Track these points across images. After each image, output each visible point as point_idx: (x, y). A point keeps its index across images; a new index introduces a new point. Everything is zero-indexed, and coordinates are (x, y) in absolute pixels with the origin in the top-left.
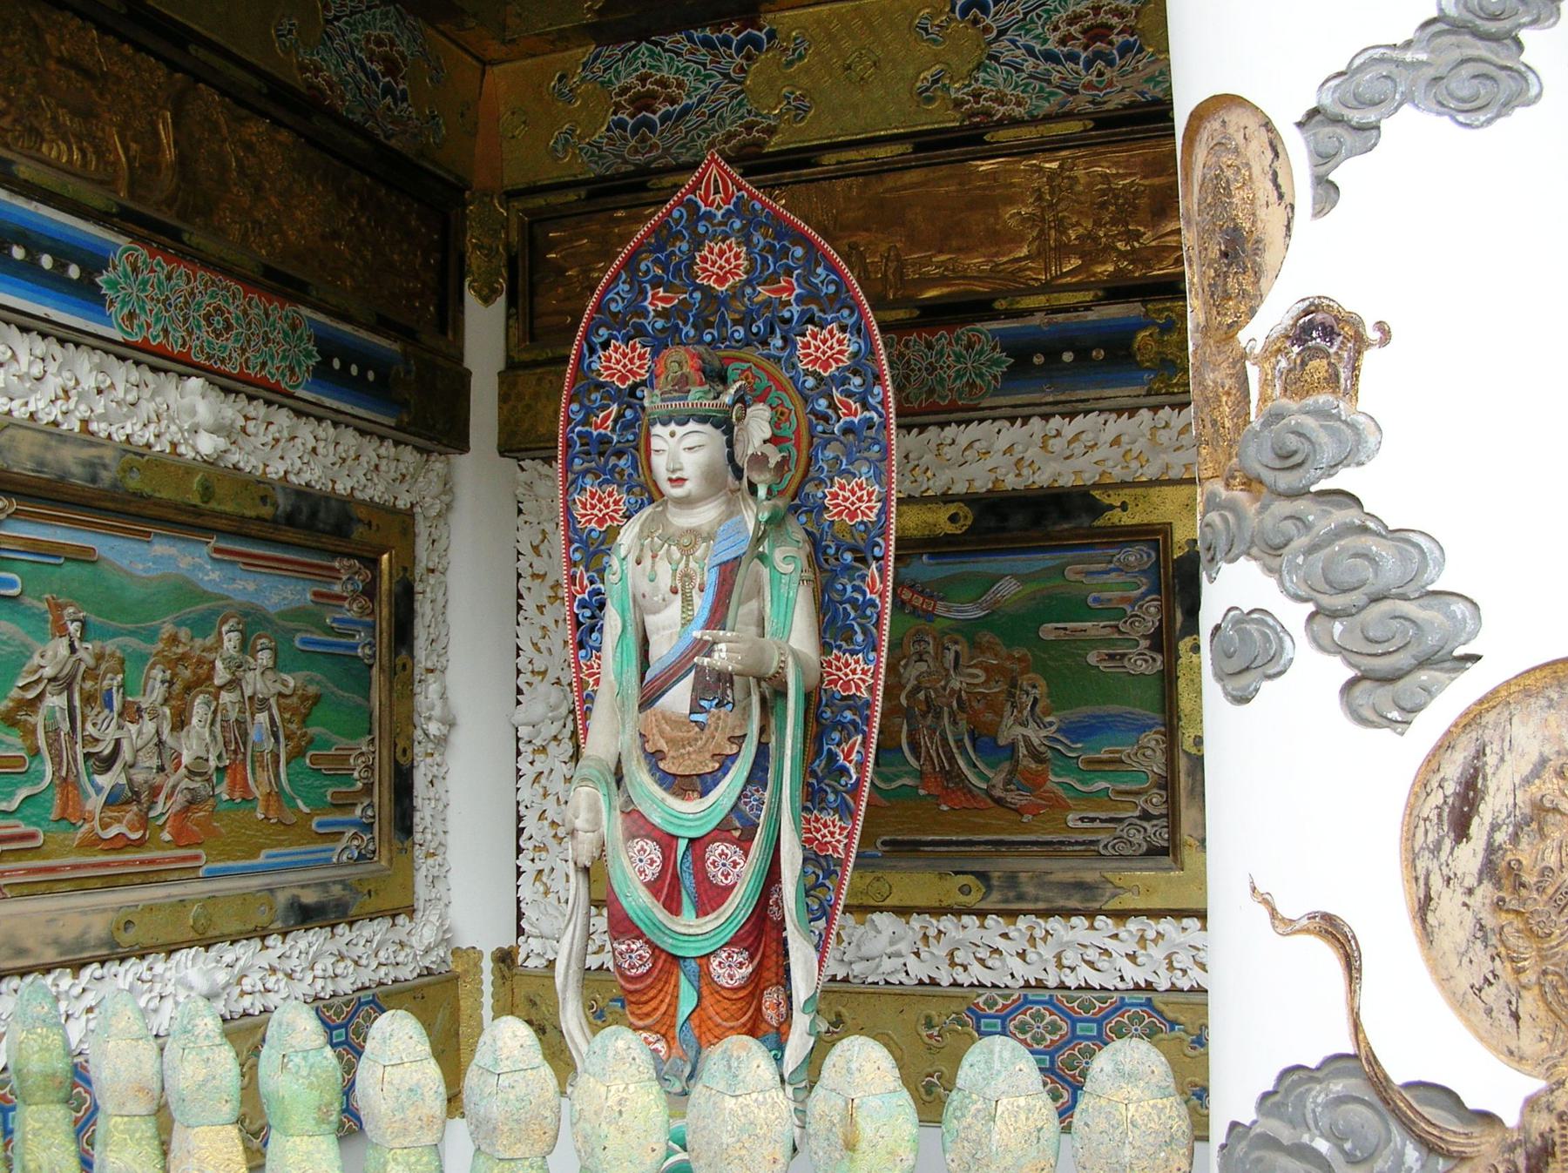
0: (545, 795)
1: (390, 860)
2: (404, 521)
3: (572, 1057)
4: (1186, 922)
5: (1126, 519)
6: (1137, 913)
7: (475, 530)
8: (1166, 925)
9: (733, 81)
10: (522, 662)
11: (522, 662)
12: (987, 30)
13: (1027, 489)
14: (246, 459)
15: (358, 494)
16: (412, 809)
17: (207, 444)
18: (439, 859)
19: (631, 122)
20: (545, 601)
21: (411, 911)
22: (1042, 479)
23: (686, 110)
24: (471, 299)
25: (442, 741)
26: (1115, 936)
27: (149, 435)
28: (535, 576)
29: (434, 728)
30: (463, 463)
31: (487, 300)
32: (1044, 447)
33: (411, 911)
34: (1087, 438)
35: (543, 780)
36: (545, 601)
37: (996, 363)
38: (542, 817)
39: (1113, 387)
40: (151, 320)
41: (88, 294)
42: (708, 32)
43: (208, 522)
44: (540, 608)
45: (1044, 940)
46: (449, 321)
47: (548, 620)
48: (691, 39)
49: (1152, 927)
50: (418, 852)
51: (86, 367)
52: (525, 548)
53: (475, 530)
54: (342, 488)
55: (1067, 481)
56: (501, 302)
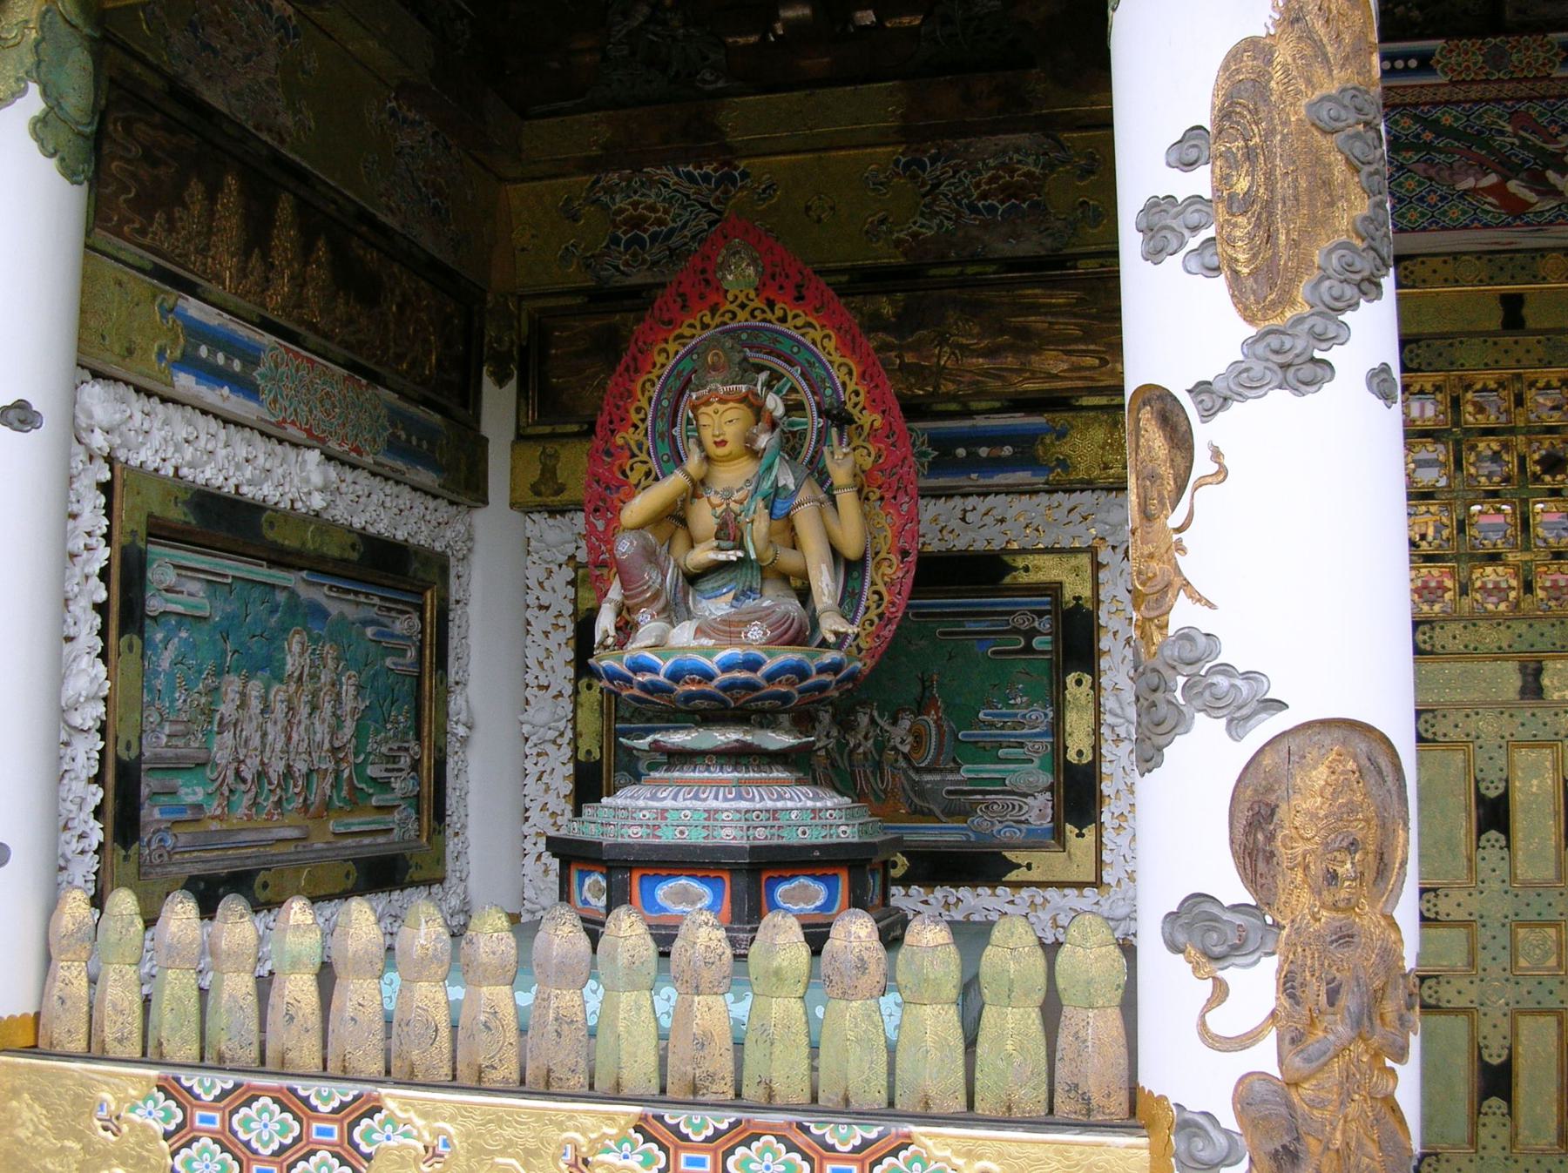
0: (547, 790)
1: (428, 839)
2: (438, 566)
3: (1477, 808)
4: (1067, 891)
5: (1024, 578)
6: (1029, 884)
7: (502, 573)
8: (1051, 893)
9: (711, 210)
10: (530, 678)
11: (530, 678)
12: (923, 184)
13: (948, 550)
14: (340, 513)
15: (411, 540)
16: (445, 795)
17: (317, 502)
18: (462, 838)
19: (624, 238)
20: (549, 628)
21: (441, 881)
22: (960, 544)
23: (672, 232)
24: (488, 383)
25: (464, 741)
26: (1012, 902)
27: (219, 481)
28: (541, 607)
29: (461, 730)
30: (480, 517)
31: (501, 381)
32: (963, 519)
33: (441, 881)
34: (997, 513)
35: (545, 778)
36: (549, 628)
37: (925, 454)
38: (544, 808)
39: (1003, 471)
40: (287, 404)
41: (245, 386)
42: (691, 168)
43: (288, 559)
44: (546, 634)
45: (956, 905)
46: (470, 398)
47: (551, 644)
48: (677, 174)
49: (1039, 894)
50: (449, 832)
51: (243, 445)
52: (532, 583)
53: (502, 573)
54: (400, 535)
55: (980, 546)
56: (512, 385)
